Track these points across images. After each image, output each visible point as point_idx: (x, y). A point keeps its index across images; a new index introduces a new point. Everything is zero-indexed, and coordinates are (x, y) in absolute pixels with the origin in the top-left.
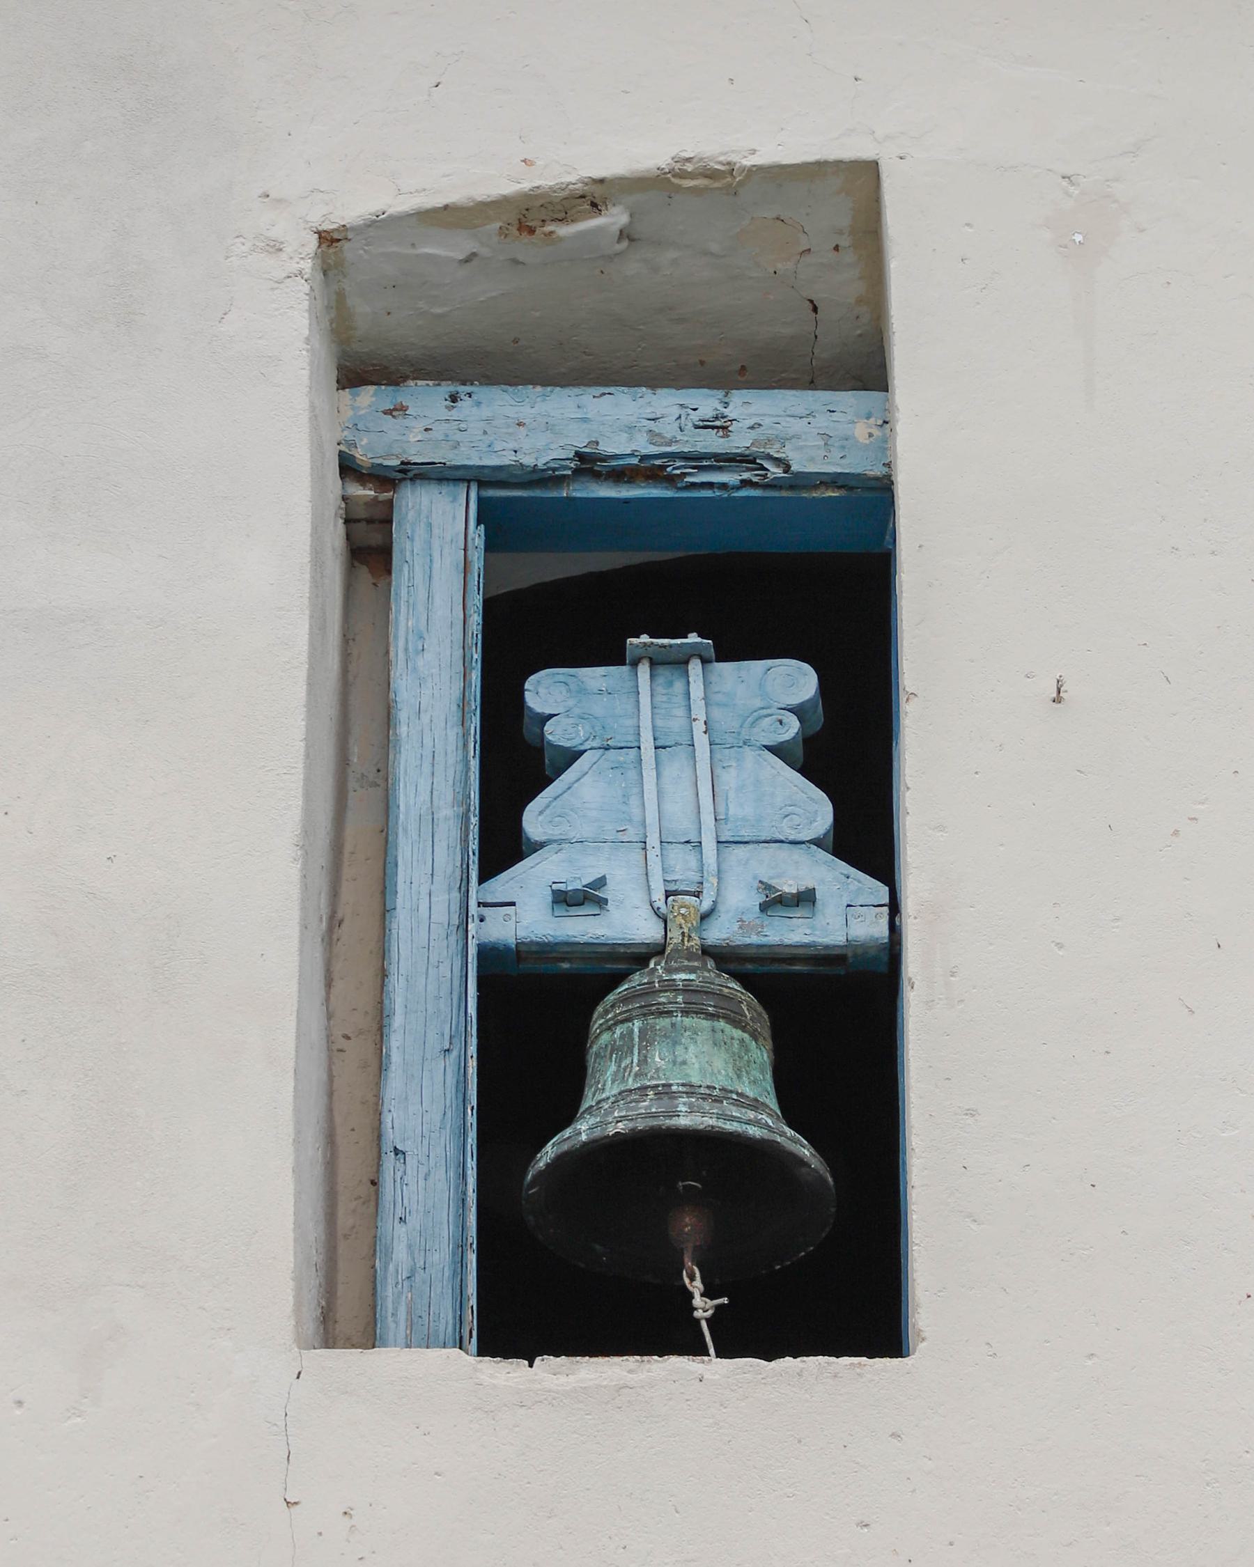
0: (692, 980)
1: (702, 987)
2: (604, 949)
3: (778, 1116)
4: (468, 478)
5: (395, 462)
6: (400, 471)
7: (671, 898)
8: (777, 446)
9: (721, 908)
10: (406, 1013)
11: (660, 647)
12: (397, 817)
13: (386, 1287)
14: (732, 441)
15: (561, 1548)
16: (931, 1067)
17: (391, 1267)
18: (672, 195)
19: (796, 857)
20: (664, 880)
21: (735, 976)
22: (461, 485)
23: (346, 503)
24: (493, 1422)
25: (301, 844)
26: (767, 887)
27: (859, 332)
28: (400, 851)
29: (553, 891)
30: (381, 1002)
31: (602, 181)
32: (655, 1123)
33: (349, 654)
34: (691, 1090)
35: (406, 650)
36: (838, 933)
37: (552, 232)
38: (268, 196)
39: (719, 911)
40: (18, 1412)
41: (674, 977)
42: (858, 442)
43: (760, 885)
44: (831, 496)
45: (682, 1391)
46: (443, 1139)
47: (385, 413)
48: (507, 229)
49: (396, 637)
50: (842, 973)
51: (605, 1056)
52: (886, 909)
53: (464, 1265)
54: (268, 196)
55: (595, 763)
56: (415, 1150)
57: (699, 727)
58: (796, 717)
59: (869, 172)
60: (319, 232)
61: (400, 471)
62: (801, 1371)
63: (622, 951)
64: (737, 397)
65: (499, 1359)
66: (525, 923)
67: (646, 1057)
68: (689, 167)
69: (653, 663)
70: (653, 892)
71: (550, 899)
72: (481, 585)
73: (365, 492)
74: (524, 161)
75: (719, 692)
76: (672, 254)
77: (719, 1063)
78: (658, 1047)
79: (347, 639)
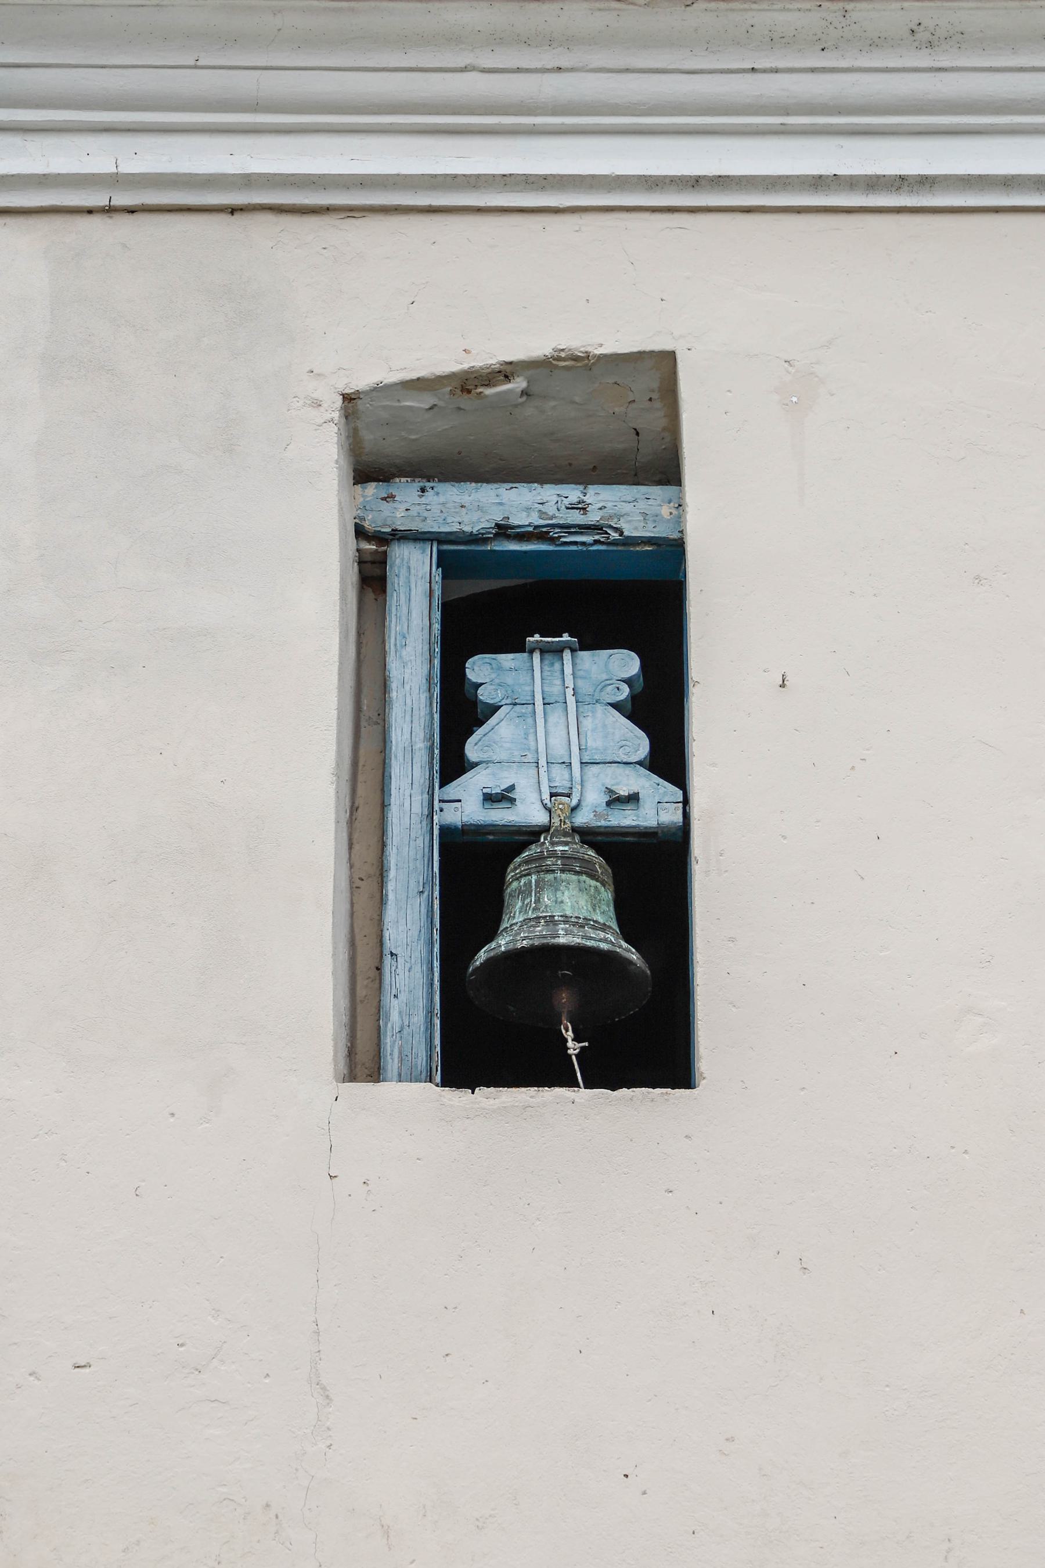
0: (567, 851)
1: (573, 855)
2: (514, 828)
3: (618, 933)
4: (432, 538)
5: (388, 530)
6: (391, 535)
7: (553, 798)
8: (616, 520)
9: (583, 804)
10: (397, 869)
11: (546, 643)
12: (391, 748)
13: (386, 1037)
14: (589, 517)
15: (491, 1204)
16: (708, 911)
17: (389, 1025)
18: (553, 370)
19: (627, 772)
20: (550, 786)
21: (592, 845)
22: (427, 543)
23: (359, 553)
24: (451, 1128)
25: (335, 773)
26: (610, 791)
27: (663, 447)
28: (393, 769)
29: (484, 794)
30: (382, 861)
31: (511, 363)
32: (545, 941)
33: (361, 643)
34: (566, 919)
35: (396, 645)
36: (652, 819)
37: (481, 393)
38: (312, 372)
39: (582, 806)
40: (172, 1120)
41: (556, 849)
42: (663, 518)
43: (606, 790)
44: (647, 550)
45: (562, 1109)
46: (419, 946)
47: (382, 499)
48: (455, 391)
49: (389, 637)
50: (655, 841)
51: (515, 896)
52: (681, 805)
53: (432, 1024)
54: (312, 372)
55: (508, 713)
56: (403, 954)
57: (569, 692)
58: (627, 685)
59: (668, 359)
60: (343, 395)
61: (391, 535)
62: (632, 1097)
63: (524, 829)
64: (592, 489)
65: (454, 1089)
66: (466, 813)
67: (539, 898)
68: (563, 355)
69: (543, 652)
70: (543, 794)
71: (482, 798)
72: (440, 605)
73: (369, 547)
74: (465, 351)
75: (581, 670)
76: (552, 403)
77: (582, 903)
78: (546, 892)
79: (360, 634)
